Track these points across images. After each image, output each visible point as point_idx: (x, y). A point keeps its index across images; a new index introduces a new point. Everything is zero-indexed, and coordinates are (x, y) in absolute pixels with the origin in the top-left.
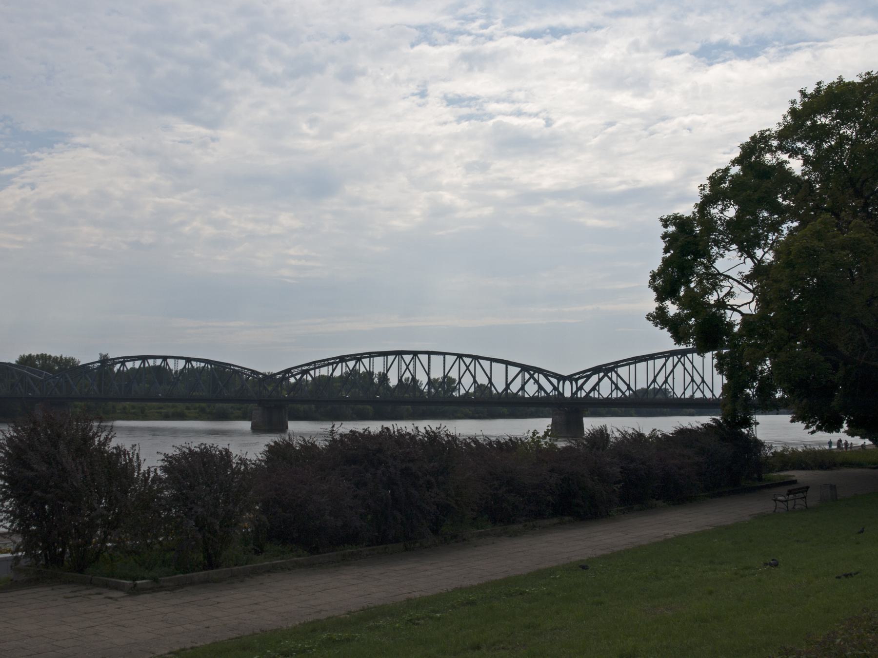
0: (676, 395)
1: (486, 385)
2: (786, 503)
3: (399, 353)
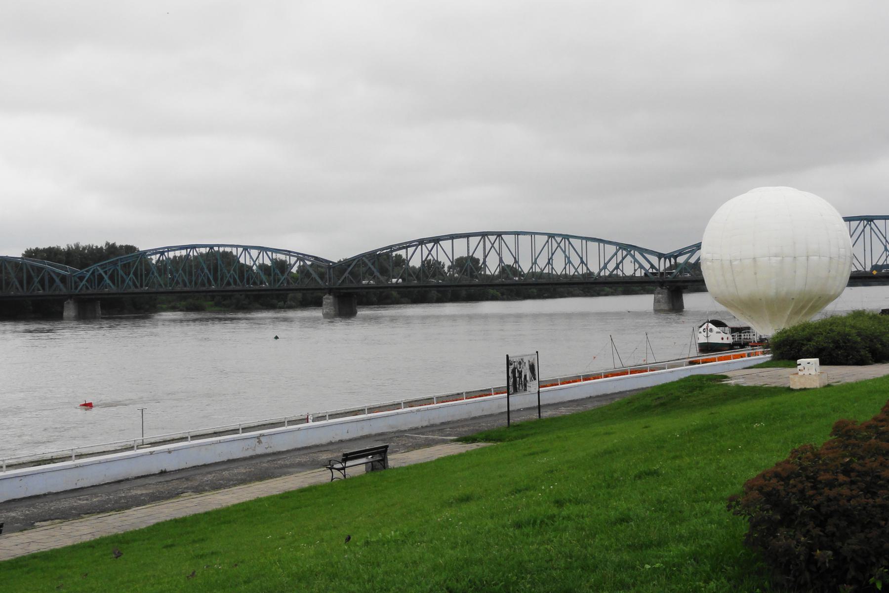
0: (555, 271)
1: (512, 265)
2: (343, 471)
3: (484, 235)
